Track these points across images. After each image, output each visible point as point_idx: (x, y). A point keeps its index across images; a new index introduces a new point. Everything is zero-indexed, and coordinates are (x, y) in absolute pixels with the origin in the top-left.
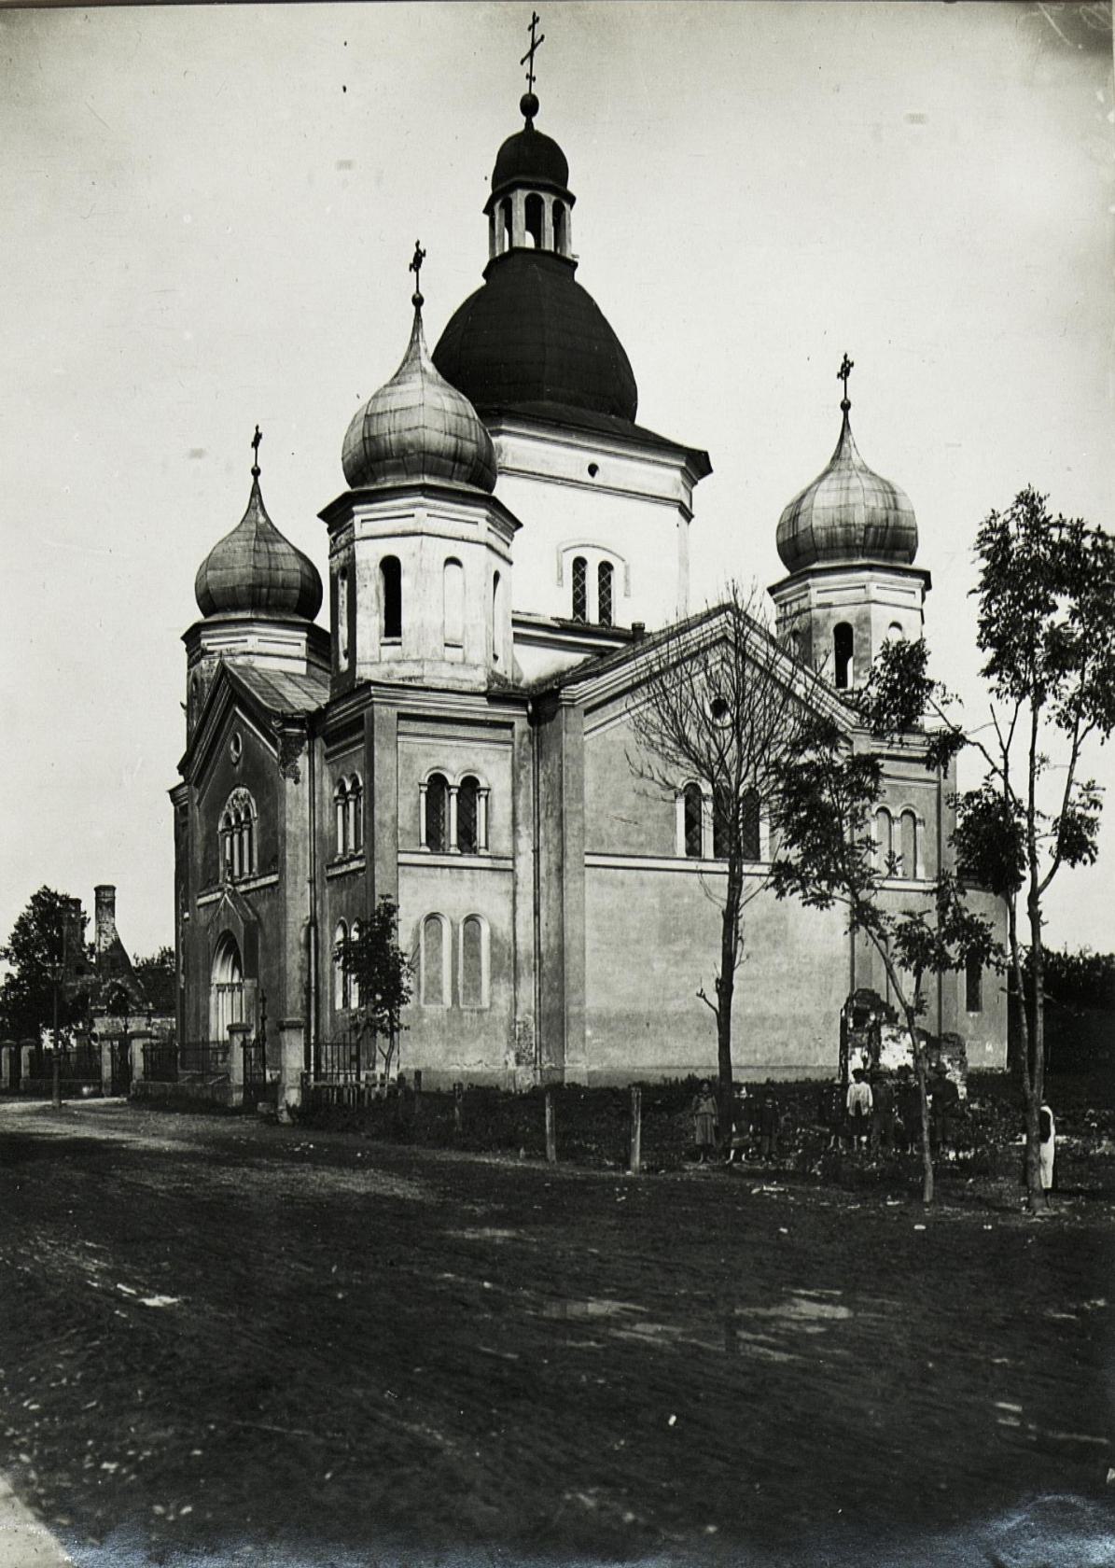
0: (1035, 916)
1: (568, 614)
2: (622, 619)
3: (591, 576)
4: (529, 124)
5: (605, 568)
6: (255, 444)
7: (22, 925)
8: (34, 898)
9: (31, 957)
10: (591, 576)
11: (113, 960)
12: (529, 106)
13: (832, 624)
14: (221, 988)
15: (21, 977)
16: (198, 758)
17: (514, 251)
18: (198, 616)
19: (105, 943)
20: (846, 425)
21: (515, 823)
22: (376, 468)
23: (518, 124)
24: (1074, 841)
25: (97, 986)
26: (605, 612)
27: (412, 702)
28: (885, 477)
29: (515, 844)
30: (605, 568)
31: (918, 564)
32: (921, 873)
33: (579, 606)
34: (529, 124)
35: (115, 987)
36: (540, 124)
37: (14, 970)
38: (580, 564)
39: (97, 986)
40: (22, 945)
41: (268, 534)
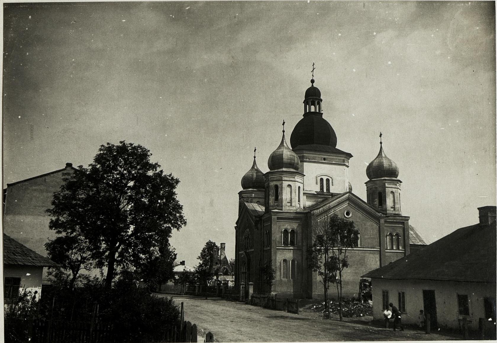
0: (340, 275)
1: (319, 190)
2: (332, 190)
3: (325, 183)
4: (312, 85)
5: (328, 180)
6: (255, 151)
7: (204, 250)
8: (207, 243)
9: (205, 259)
10: (325, 183)
11: (224, 261)
12: (313, 81)
13: (378, 192)
14: (243, 273)
15: (203, 264)
16: (240, 221)
17: (310, 112)
18: (241, 189)
19: (222, 257)
20: (381, 147)
21: (302, 239)
22: (276, 161)
23: (310, 85)
24: (345, 265)
25: (220, 268)
26: (328, 189)
27: (280, 216)
28: (390, 158)
29: (302, 244)
30: (328, 180)
31: (398, 178)
32: (401, 248)
33: (322, 188)
34: (312, 85)
35: (225, 268)
36: (315, 85)
37: (201, 262)
38: (322, 180)
39: (220, 268)
40: (203, 256)
41: (258, 171)
